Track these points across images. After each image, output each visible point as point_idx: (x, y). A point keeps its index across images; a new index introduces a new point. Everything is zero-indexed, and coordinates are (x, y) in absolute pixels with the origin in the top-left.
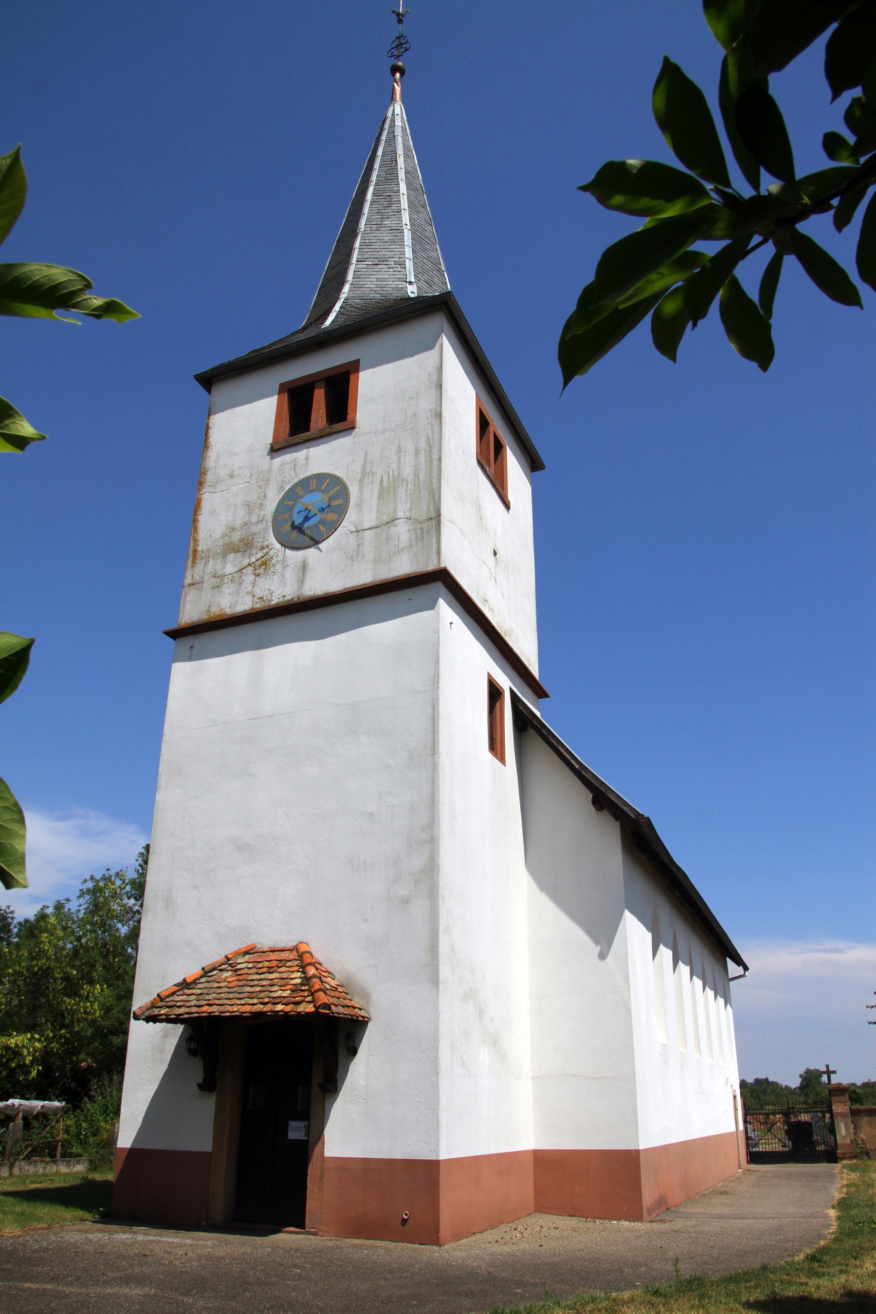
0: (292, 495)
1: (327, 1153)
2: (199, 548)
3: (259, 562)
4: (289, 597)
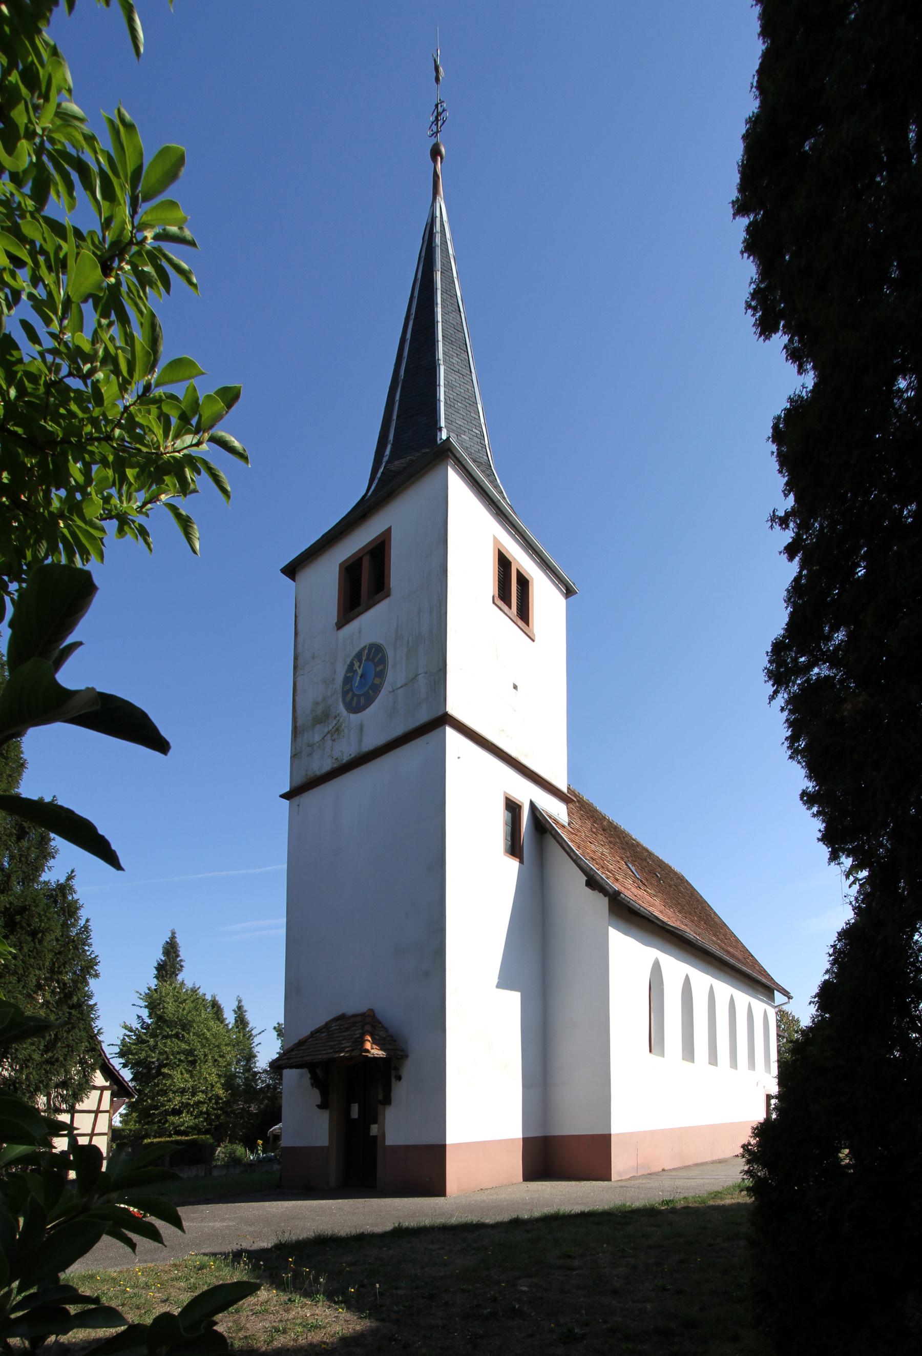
1: (387, 1144)
3: (334, 729)
4: (353, 755)
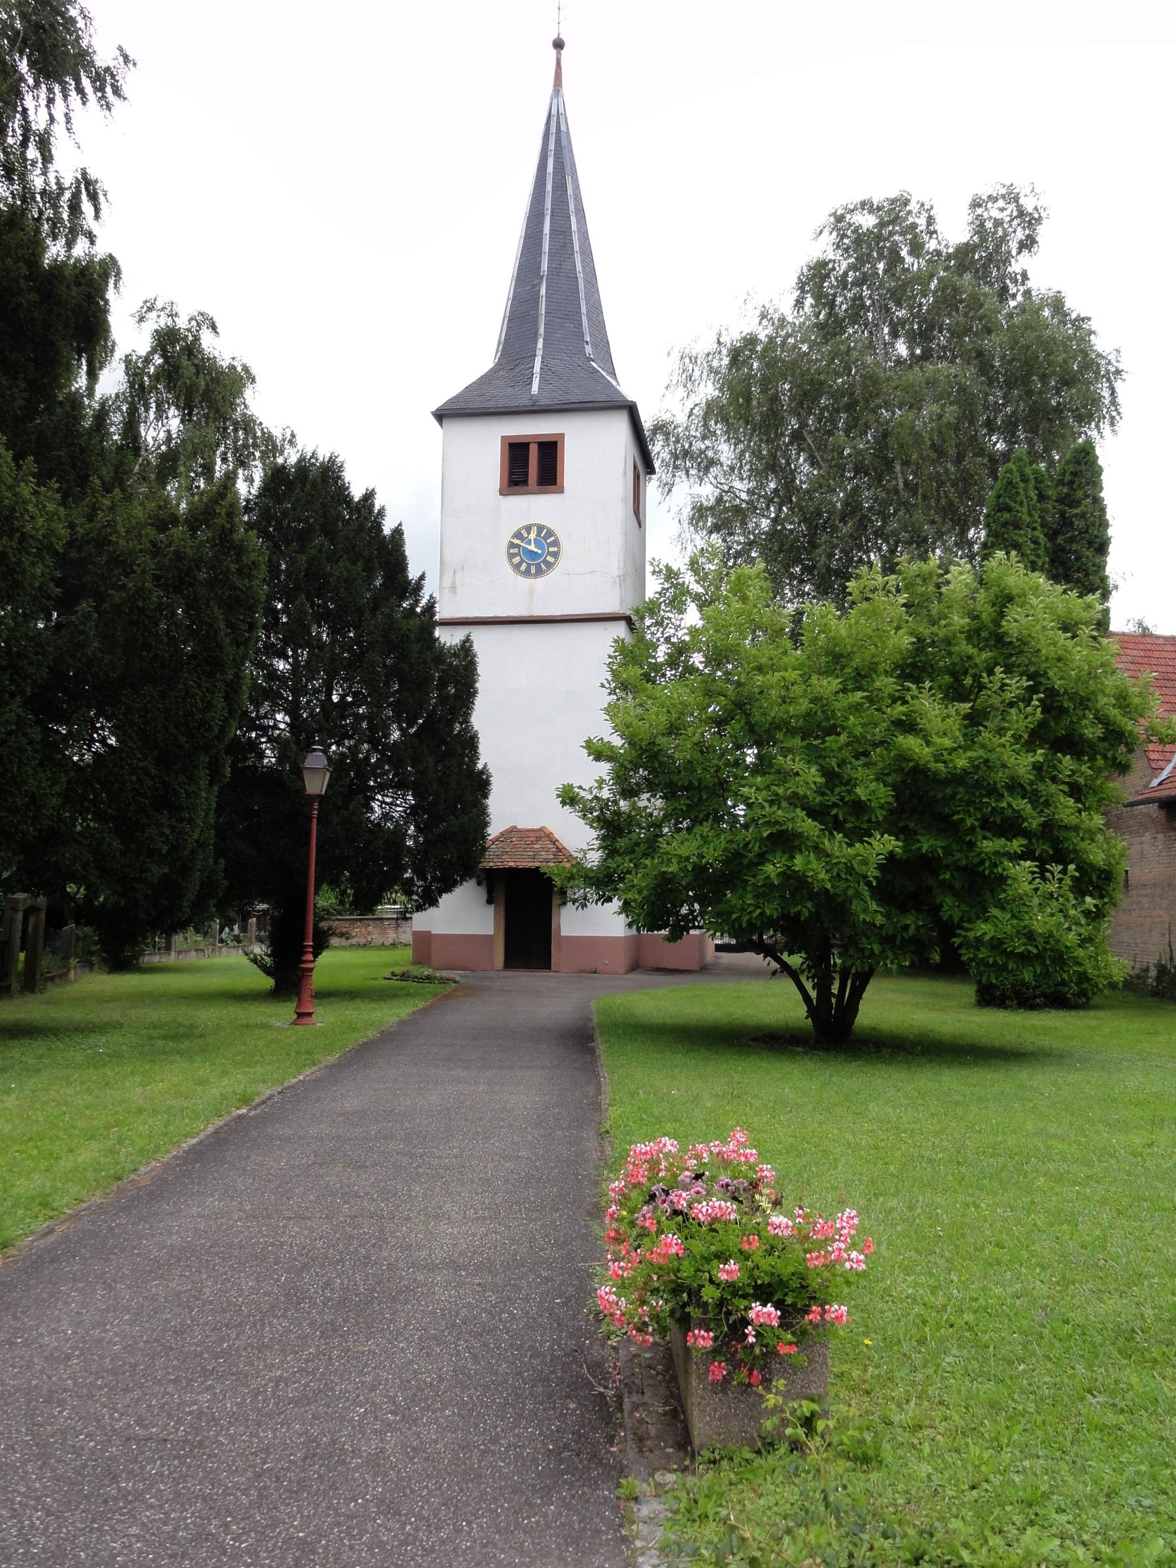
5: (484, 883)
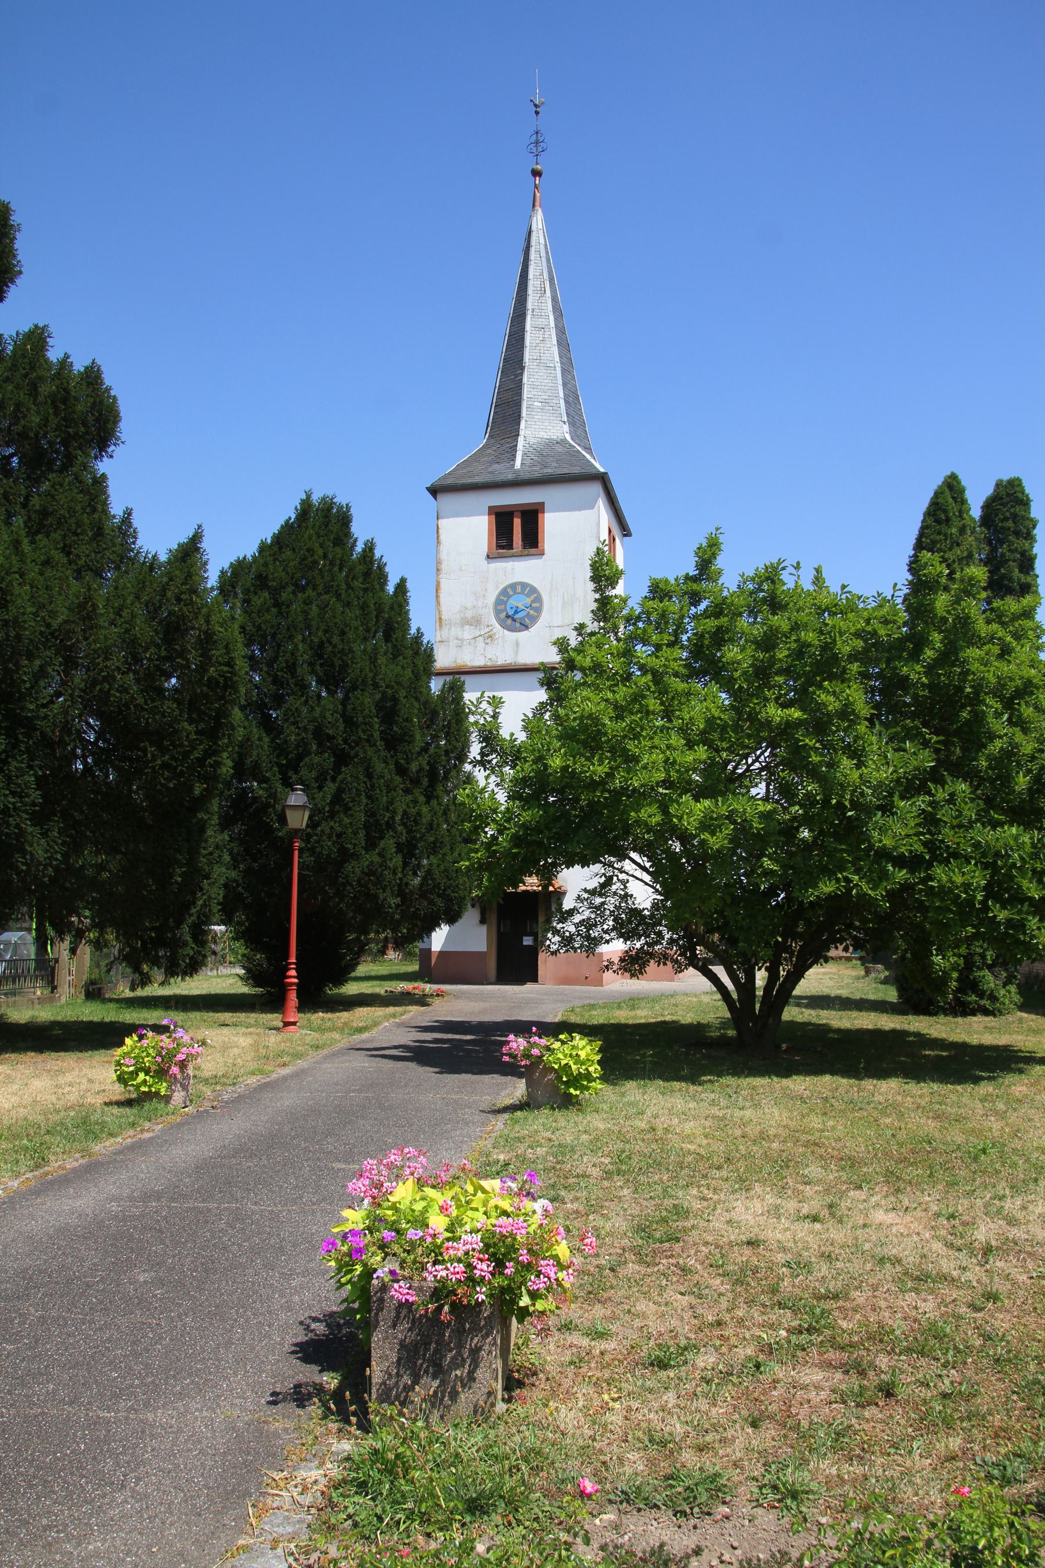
0: (505, 594)
2: (443, 617)
4: (508, 662)
5: (477, 905)
